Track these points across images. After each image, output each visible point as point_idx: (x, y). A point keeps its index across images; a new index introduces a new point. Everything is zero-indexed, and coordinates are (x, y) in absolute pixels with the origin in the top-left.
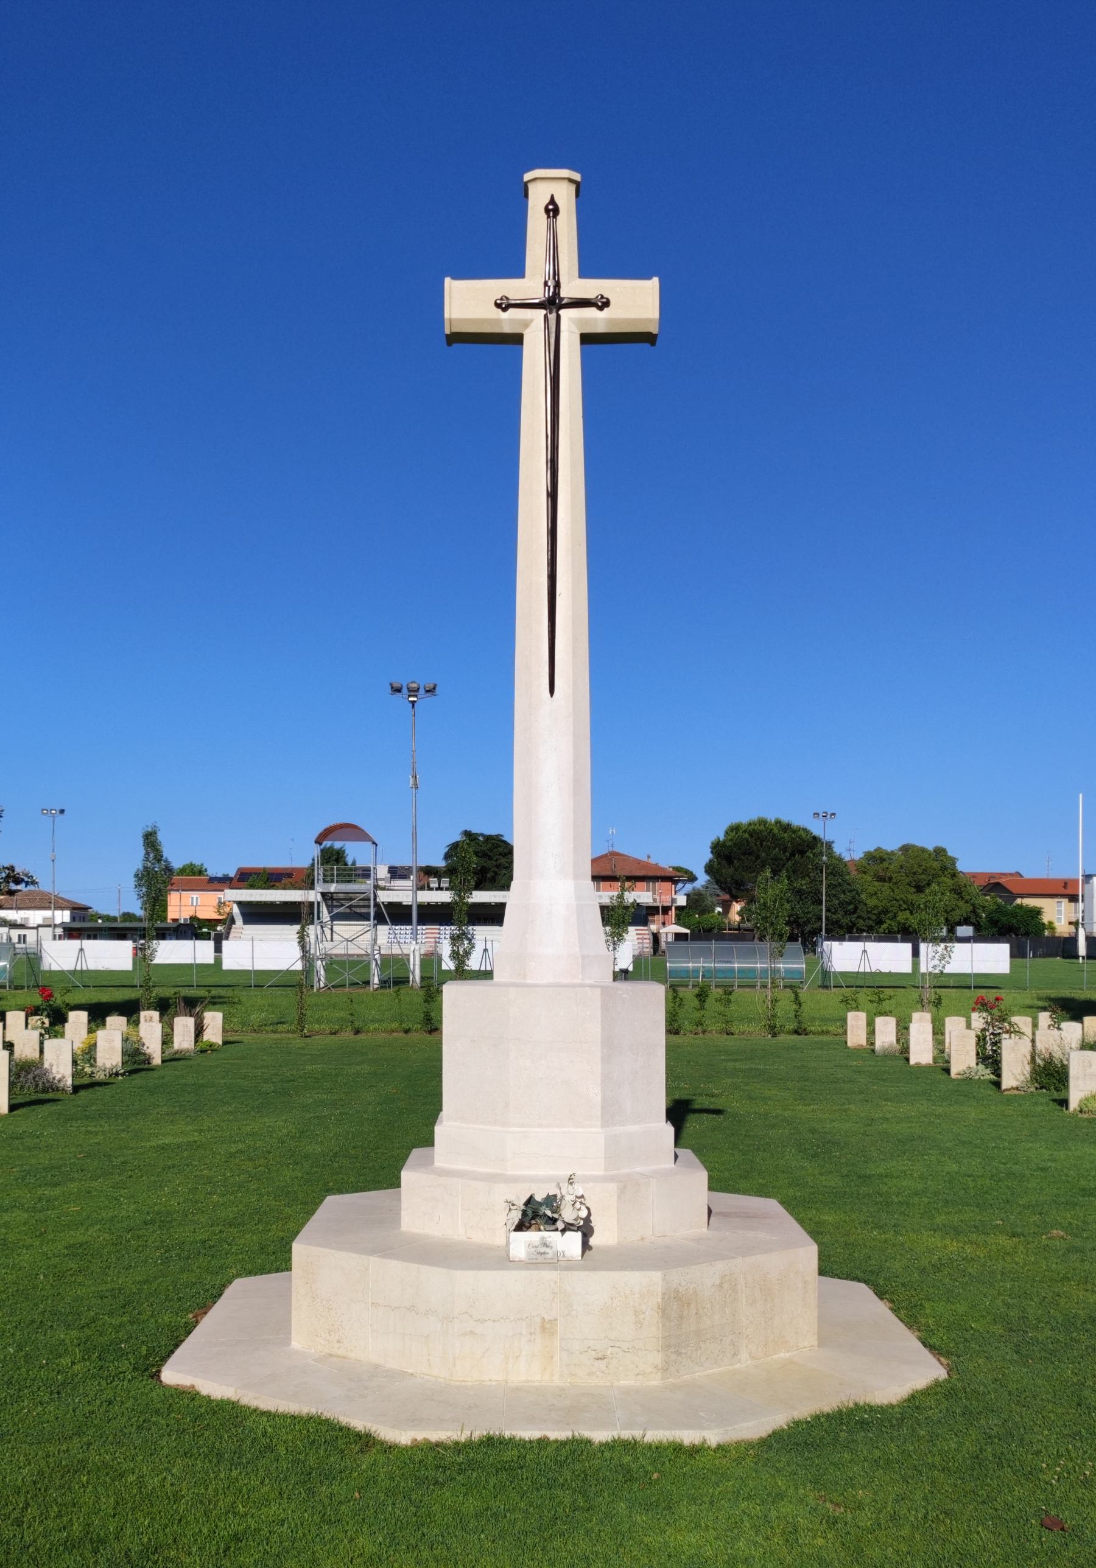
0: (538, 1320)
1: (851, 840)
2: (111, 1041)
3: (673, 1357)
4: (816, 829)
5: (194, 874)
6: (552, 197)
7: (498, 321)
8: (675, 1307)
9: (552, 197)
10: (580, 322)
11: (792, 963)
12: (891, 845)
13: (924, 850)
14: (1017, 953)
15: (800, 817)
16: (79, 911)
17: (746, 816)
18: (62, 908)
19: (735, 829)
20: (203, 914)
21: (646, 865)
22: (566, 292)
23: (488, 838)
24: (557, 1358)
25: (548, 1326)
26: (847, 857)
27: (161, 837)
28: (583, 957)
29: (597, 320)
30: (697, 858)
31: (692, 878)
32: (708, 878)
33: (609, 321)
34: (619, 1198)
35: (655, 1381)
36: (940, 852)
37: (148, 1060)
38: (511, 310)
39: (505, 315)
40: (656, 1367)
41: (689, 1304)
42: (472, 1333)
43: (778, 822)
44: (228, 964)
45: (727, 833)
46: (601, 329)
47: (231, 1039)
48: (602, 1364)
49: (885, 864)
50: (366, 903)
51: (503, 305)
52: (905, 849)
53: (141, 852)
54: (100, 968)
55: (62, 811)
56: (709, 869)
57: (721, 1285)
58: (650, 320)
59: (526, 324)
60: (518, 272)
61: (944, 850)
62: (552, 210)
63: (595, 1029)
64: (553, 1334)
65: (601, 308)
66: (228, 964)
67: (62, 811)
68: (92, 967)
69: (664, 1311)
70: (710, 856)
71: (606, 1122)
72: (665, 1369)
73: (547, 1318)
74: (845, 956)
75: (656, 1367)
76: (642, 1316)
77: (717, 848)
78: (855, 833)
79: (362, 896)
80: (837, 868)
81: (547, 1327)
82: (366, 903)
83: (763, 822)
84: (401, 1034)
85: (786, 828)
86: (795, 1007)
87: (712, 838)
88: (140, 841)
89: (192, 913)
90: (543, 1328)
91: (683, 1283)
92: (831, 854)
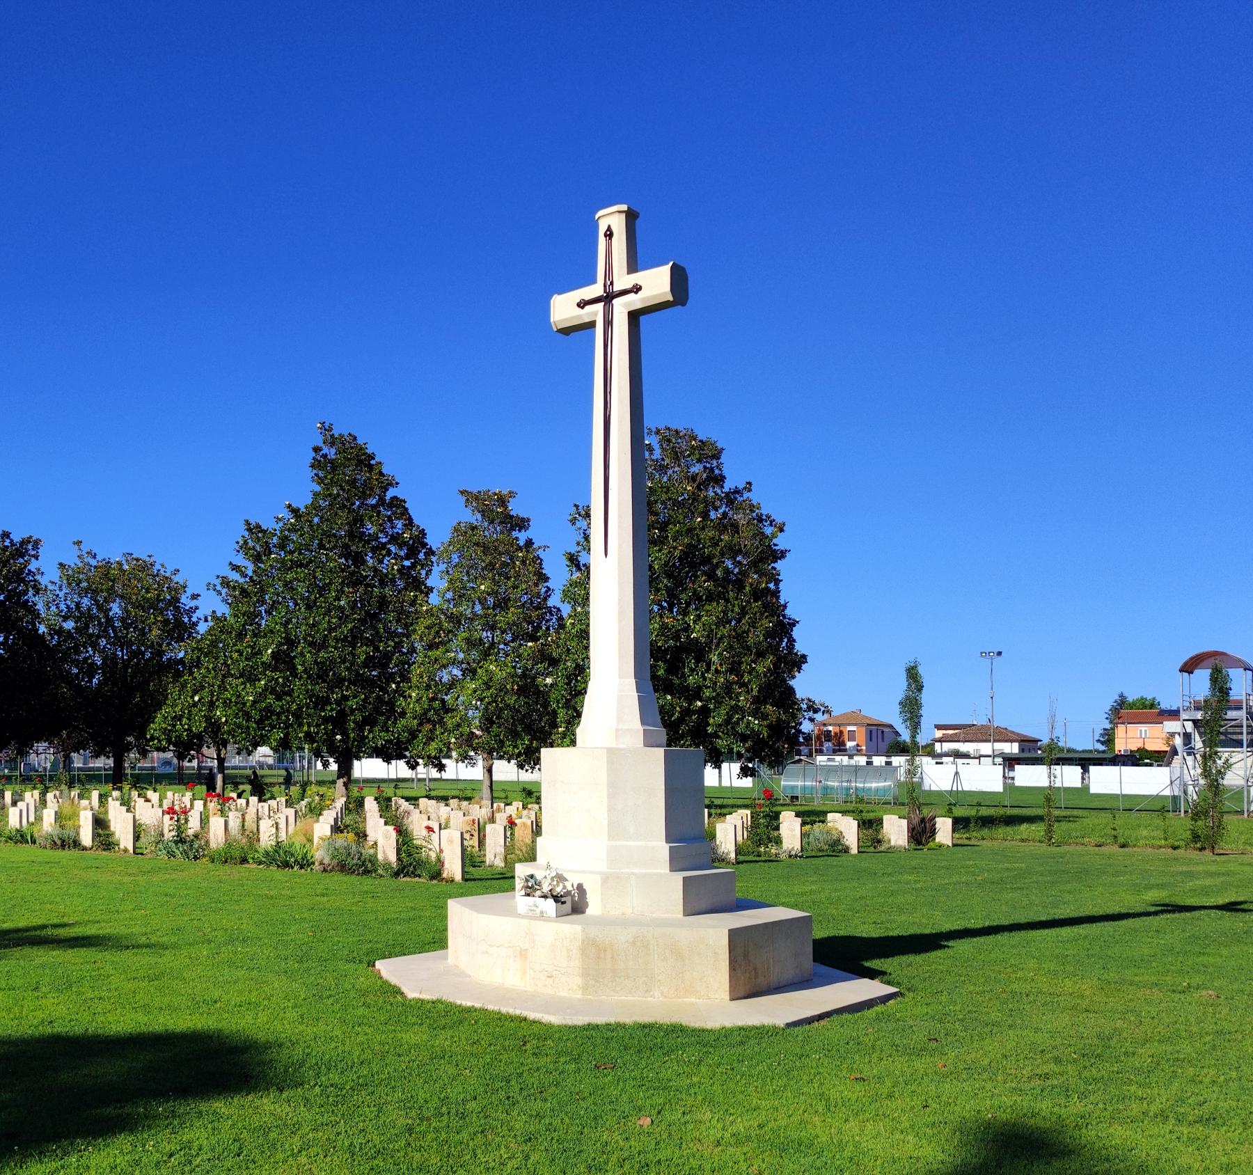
2: (792, 830)
5: (1145, 707)
7: (579, 317)
10: (625, 305)
16: (1028, 743)
18: (1012, 741)
20: (1151, 747)
22: (617, 287)
27: (921, 670)
28: (617, 730)
29: (635, 301)
33: (643, 300)
34: (602, 884)
35: (579, 996)
37: (846, 850)
44: (1094, 789)
46: (639, 306)
47: (959, 842)
48: (550, 980)
50: (1238, 730)
53: (904, 684)
54: (974, 789)
55: (1000, 653)
57: (634, 943)
58: (665, 293)
59: (596, 314)
62: (609, 234)
63: (603, 777)
66: (1094, 789)
67: (1000, 653)
68: (966, 788)
69: (584, 951)
71: (610, 837)
72: (585, 988)
79: (1233, 723)
81: (523, 954)
82: (1238, 730)
84: (1115, 849)
88: (904, 675)
89: (1140, 745)
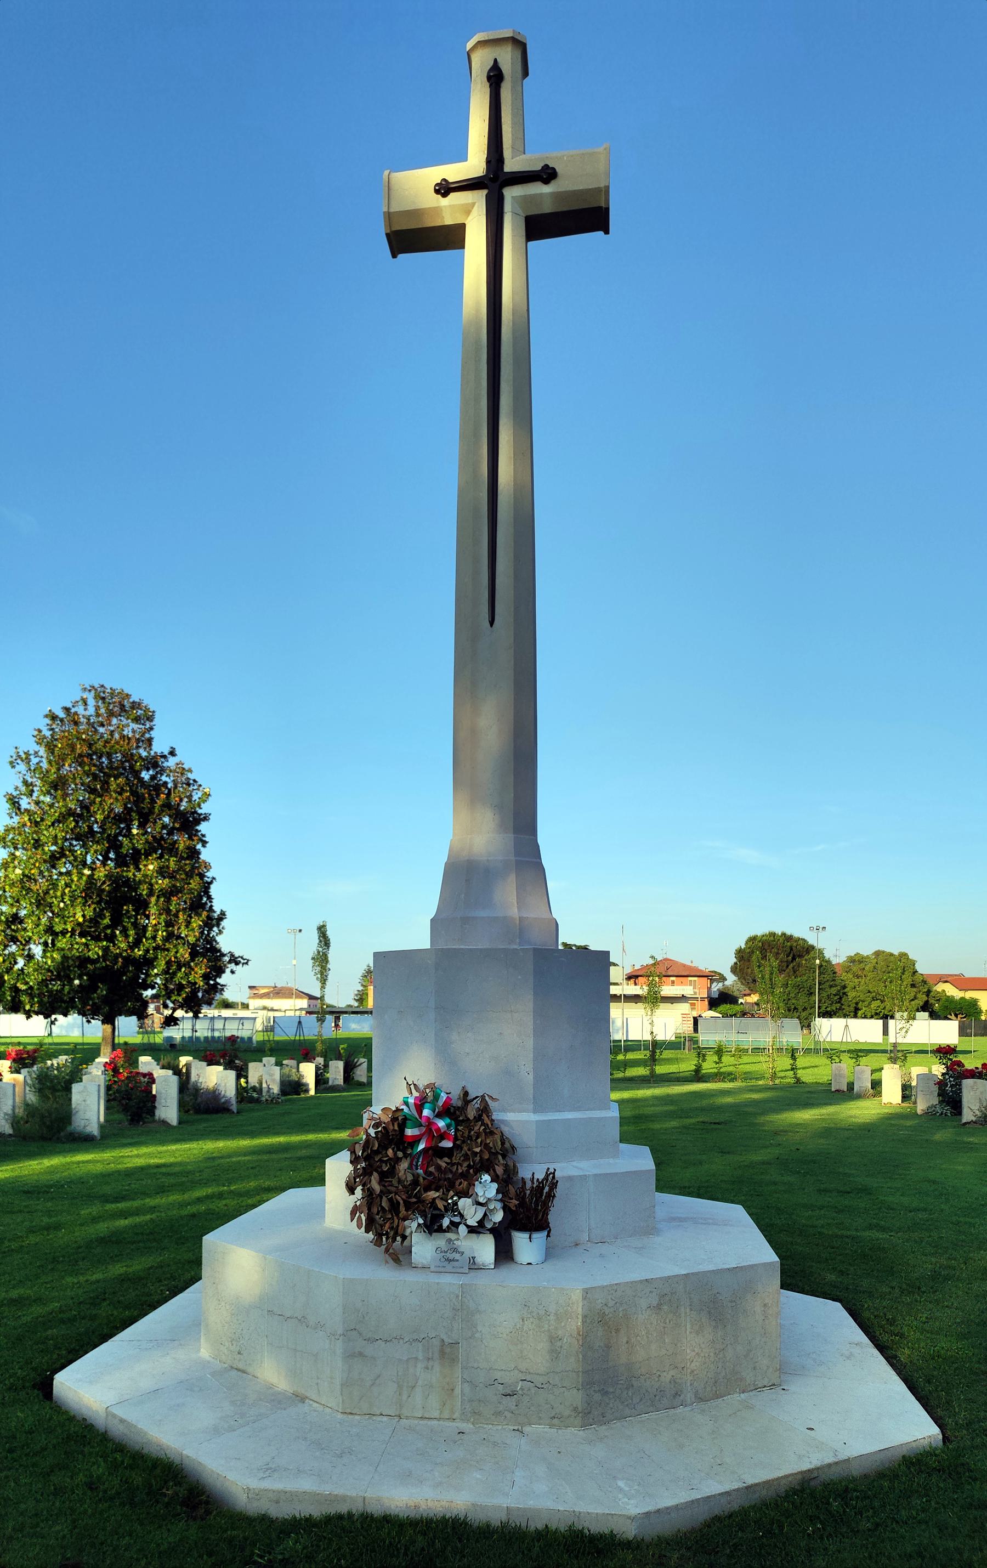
0: (436, 1342)
1: (837, 947)
3: (597, 1397)
4: (811, 939)
6: (496, 60)
7: (437, 210)
8: (600, 1334)
9: (496, 60)
11: (792, 1035)
12: (867, 950)
13: (892, 955)
14: (963, 1032)
15: (799, 930)
17: (760, 930)
19: (752, 939)
21: (690, 968)
23: (579, 947)
24: (458, 1391)
25: (448, 1350)
26: (834, 961)
30: (724, 962)
31: (723, 979)
32: (735, 978)
33: (557, 196)
36: (903, 955)
38: (452, 195)
39: (444, 202)
40: (575, 1409)
41: (617, 1331)
42: (361, 1354)
43: (783, 934)
45: (747, 943)
46: (547, 208)
49: (862, 965)
51: (444, 189)
52: (878, 954)
55: (300, 931)
56: (734, 970)
60: (464, 158)
61: (906, 955)
64: (453, 1360)
65: (546, 182)
67: (300, 931)
70: (735, 960)
73: (446, 1340)
74: (832, 1030)
75: (575, 1409)
76: (559, 1344)
77: (740, 954)
78: (840, 941)
80: (826, 966)
83: (773, 934)
85: (789, 938)
86: (792, 1062)
87: (737, 947)
90: (442, 1353)
91: (611, 1304)
92: (822, 958)
